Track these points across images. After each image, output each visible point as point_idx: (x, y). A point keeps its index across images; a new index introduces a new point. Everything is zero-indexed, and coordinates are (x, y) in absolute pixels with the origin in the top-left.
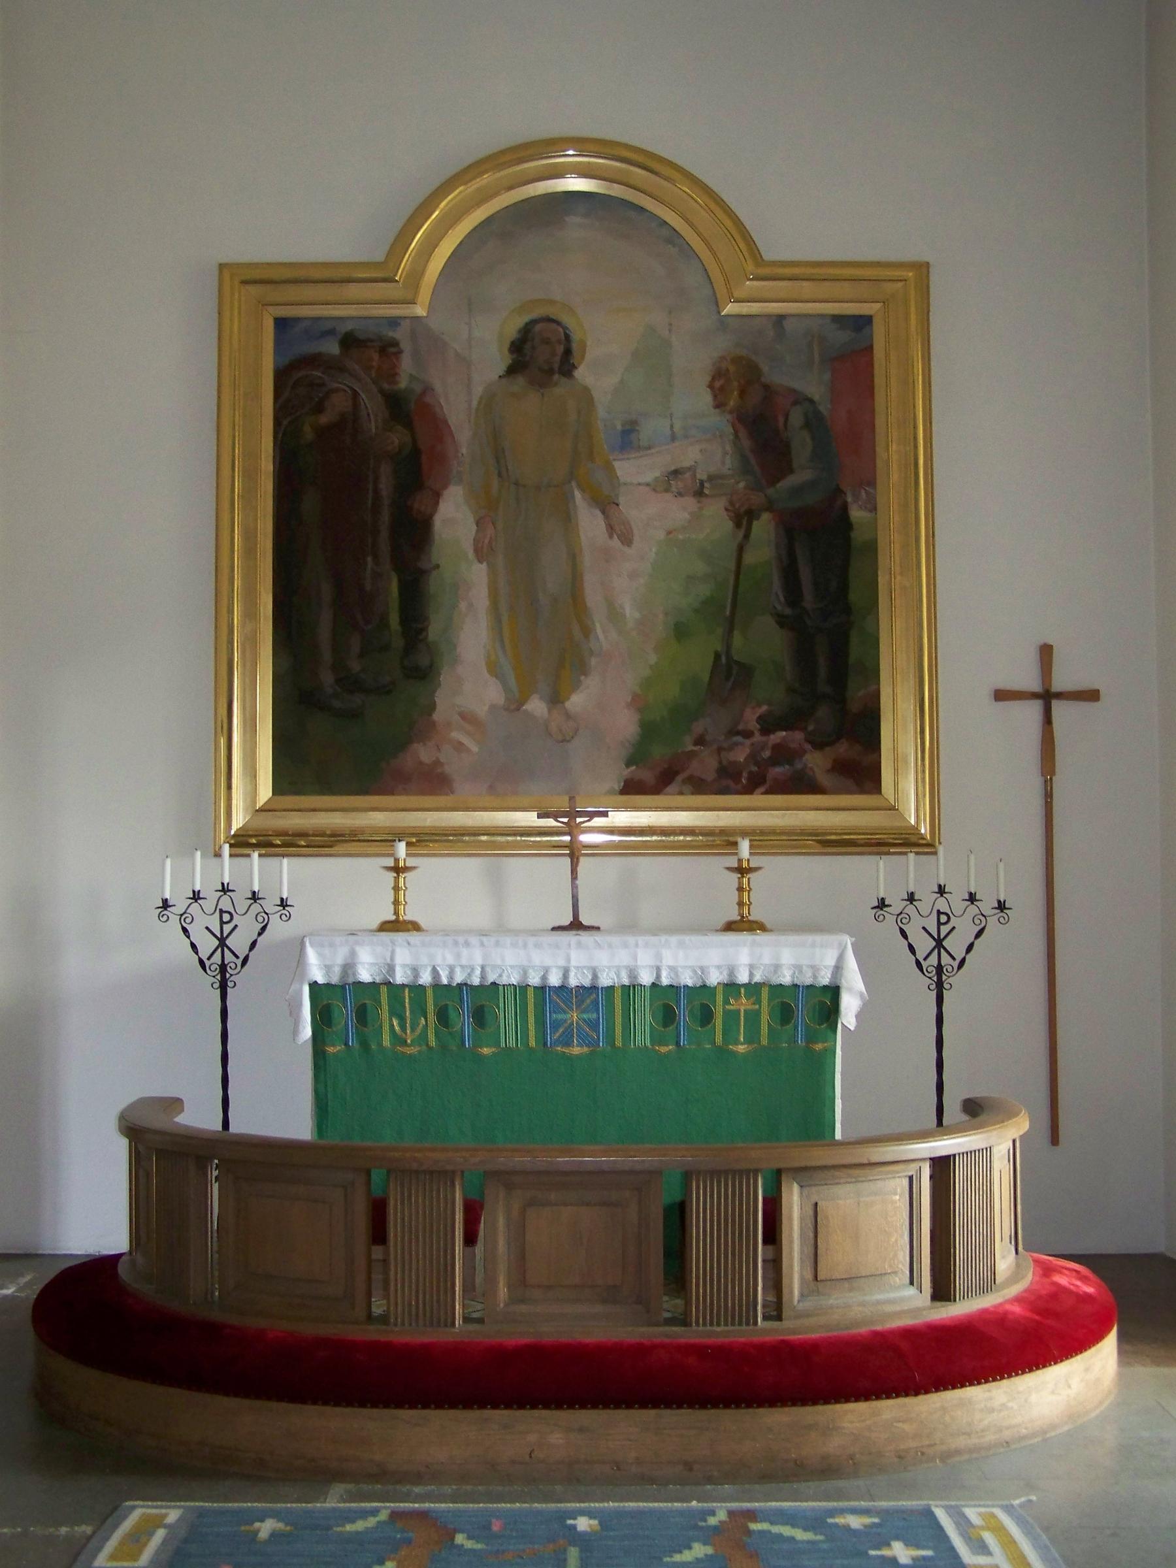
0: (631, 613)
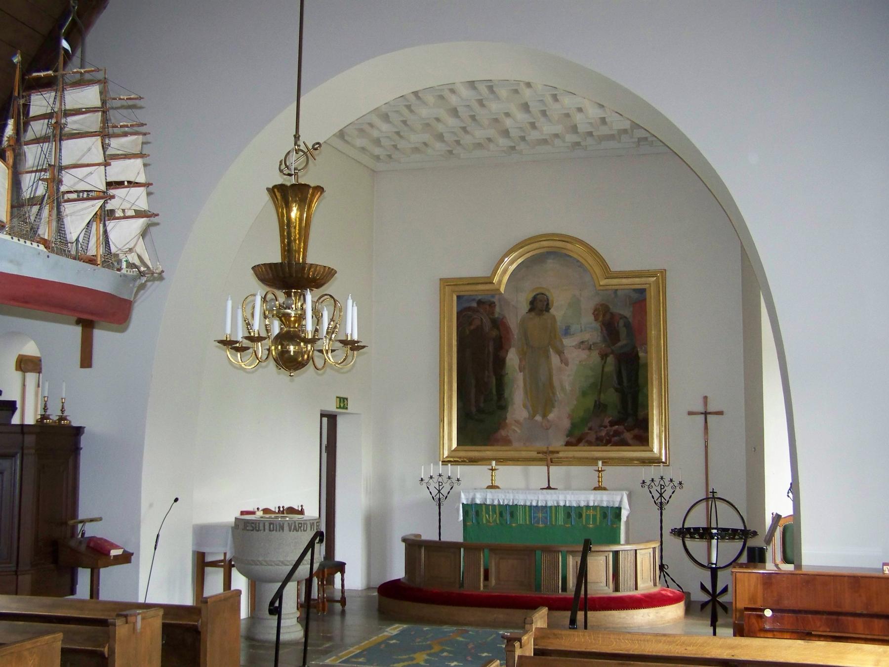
0: (568, 388)
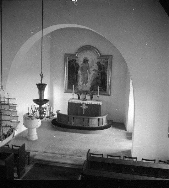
0: (91, 79)
